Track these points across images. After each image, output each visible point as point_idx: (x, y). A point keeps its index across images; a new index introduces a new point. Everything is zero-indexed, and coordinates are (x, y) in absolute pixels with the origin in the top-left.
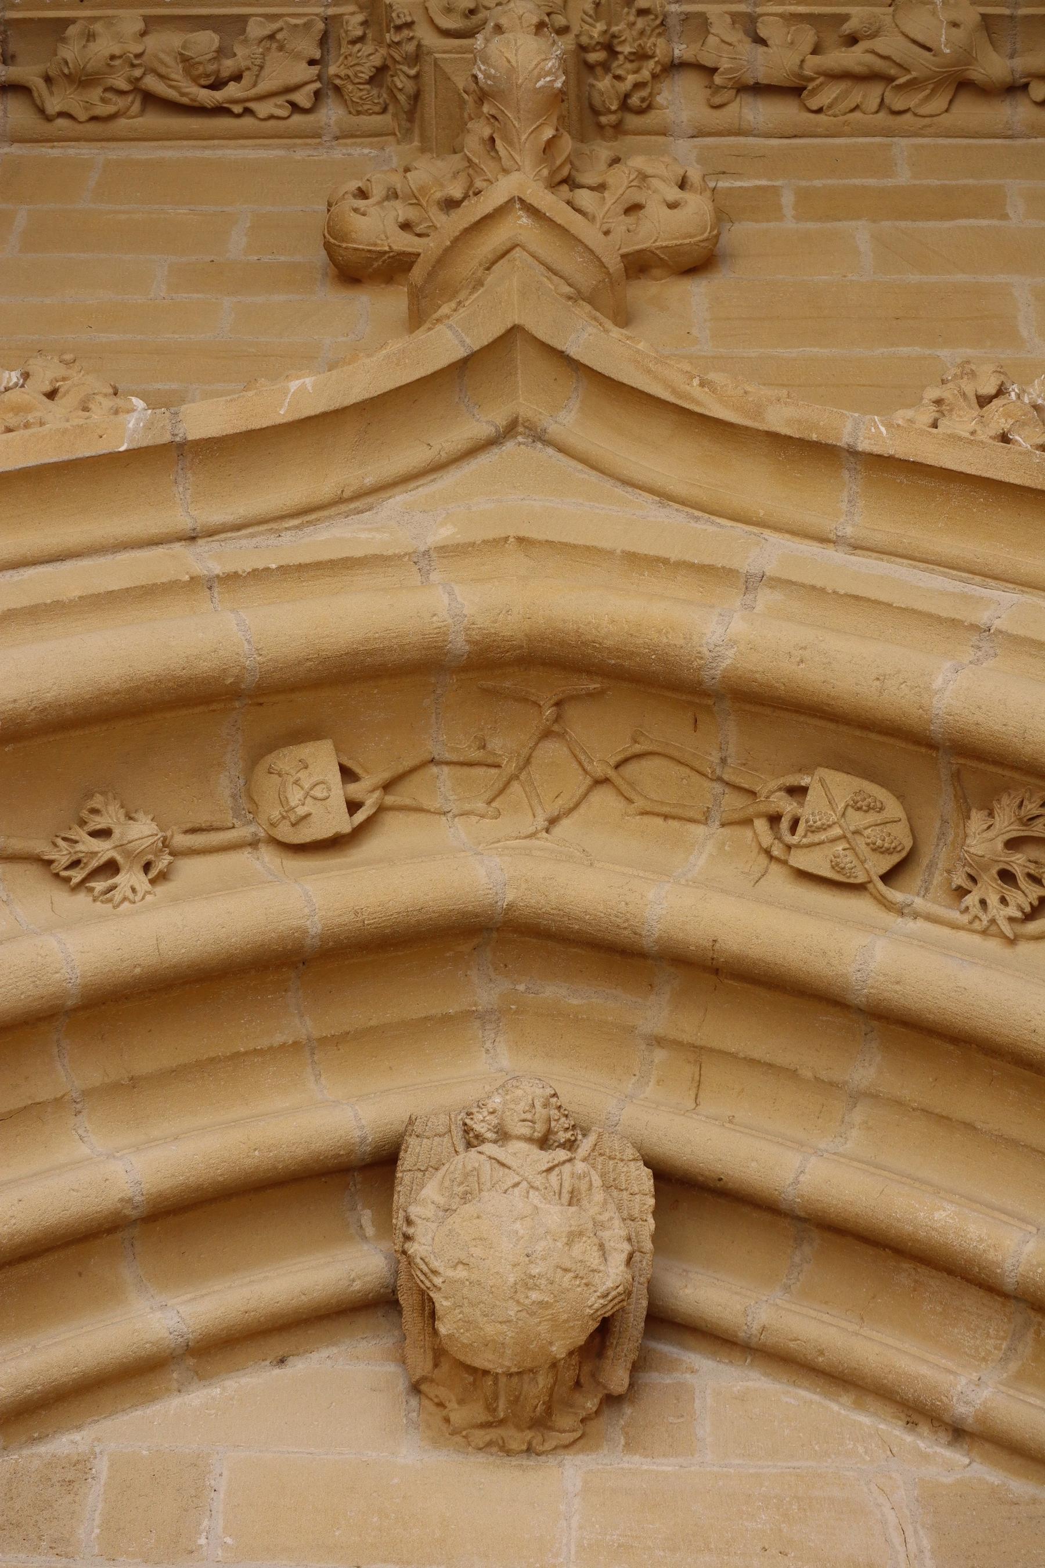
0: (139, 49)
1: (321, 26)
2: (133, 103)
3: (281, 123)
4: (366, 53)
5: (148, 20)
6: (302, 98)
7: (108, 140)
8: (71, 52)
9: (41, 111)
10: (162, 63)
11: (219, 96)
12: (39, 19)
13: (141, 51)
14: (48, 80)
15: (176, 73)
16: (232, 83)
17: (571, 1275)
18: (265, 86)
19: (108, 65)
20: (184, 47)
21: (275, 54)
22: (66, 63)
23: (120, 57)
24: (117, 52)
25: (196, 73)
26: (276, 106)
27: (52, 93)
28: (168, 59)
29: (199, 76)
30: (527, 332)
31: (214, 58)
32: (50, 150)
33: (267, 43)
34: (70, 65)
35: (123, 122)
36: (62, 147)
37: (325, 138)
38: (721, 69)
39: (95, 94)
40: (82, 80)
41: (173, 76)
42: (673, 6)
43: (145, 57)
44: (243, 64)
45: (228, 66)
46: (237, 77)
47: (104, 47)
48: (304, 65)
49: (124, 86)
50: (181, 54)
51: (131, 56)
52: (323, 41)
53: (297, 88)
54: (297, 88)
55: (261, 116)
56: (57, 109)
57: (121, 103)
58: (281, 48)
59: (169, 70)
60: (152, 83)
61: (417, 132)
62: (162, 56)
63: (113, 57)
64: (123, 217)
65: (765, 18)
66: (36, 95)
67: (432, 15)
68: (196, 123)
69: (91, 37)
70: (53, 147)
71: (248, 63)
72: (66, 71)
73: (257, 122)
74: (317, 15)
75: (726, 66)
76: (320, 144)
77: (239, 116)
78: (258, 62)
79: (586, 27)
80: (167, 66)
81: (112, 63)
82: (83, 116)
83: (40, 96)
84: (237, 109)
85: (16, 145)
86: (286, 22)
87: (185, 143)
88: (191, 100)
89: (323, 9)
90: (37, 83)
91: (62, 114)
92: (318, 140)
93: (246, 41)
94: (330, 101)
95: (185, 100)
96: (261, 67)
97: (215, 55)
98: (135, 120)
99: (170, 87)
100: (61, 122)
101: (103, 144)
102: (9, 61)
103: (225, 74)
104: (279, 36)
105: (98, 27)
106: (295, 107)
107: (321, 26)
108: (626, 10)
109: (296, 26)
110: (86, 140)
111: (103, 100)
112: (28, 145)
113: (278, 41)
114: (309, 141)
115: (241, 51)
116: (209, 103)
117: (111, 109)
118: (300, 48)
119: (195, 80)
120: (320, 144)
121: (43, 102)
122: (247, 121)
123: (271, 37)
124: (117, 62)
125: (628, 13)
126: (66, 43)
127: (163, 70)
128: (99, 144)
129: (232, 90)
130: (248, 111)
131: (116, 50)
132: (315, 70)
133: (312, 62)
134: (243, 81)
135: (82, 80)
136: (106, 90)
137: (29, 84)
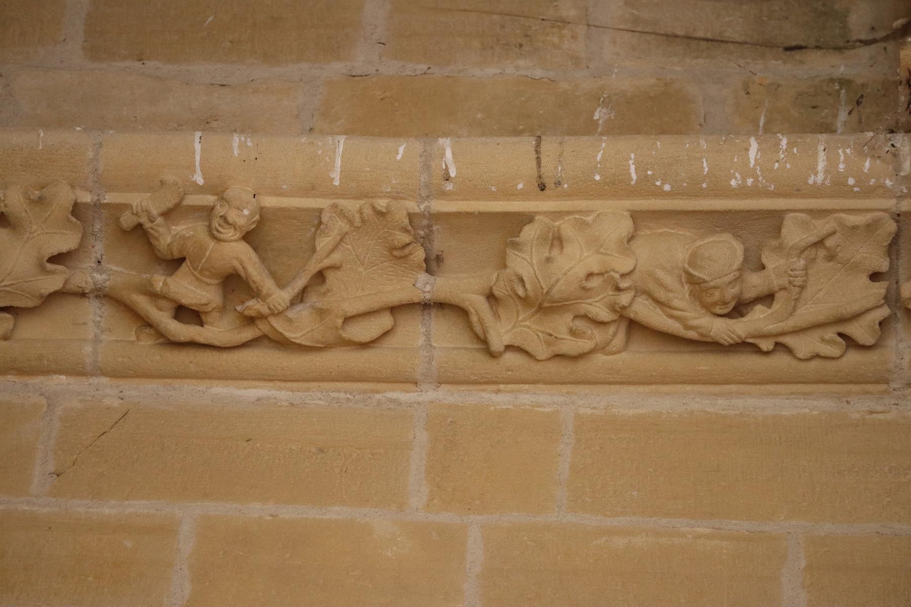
0: (625, 265)
1: (892, 227)
2: (615, 334)
3: (830, 365)
5: (636, 216)
6: (860, 331)
7: (578, 383)
8: (525, 263)
9: (483, 342)
10: (661, 285)
11: (740, 328)
12: (481, 214)
13: (630, 268)
14: (491, 297)
15: (681, 298)
16: (759, 308)
18: (807, 313)
19: (583, 288)
20: (693, 260)
21: (822, 265)
22: (521, 280)
23: (600, 274)
24: (596, 269)
25: (709, 300)
26: (823, 340)
27: (497, 316)
28: (668, 280)
29: (715, 304)
31: (736, 280)
32: (493, 397)
33: (810, 253)
34: (528, 286)
35: (600, 359)
36: (511, 392)
37: (894, 385)
39: (562, 324)
40: (544, 305)
41: (676, 303)
43: (635, 276)
44: (776, 283)
45: (755, 283)
46: (768, 298)
47: (575, 262)
48: (864, 279)
49: (604, 314)
50: (688, 274)
51: (617, 276)
52: (893, 248)
53: (855, 317)
54: (855, 317)
55: (800, 355)
56: (507, 340)
57: (599, 335)
58: (831, 257)
59: (671, 295)
60: (644, 311)
62: (661, 274)
63: (590, 275)
64: (620, 542)
66: (474, 319)
68: (705, 363)
69: (557, 240)
70: (498, 392)
71: (784, 281)
72: (521, 292)
73: (794, 363)
74: (885, 211)
76: (885, 392)
77: (767, 353)
78: (799, 281)
80: (668, 290)
81: (590, 284)
82: (542, 352)
83: (481, 322)
84: (766, 345)
85: (445, 387)
86: (841, 223)
87: (689, 388)
88: (701, 335)
89: (894, 201)
90: (477, 303)
91: (509, 348)
92: (883, 387)
93: (780, 248)
94: (899, 326)
95: (692, 335)
96: (802, 287)
97: (737, 274)
98: (617, 356)
99: (671, 317)
100: (511, 358)
101: (571, 388)
102: (434, 264)
103: (750, 294)
104: (829, 243)
105: (567, 228)
106: (850, 342)
107: (892, 227)
109: (855, 228)
110: (546, 383)
111: (573, 332)
112: (463, 388)
113: (826, 248)
114: (869, 387)
115: (772, 261)
116: (726, 339)
117: (584, 345)
118: (858, 257)
119: (708, 308)
120: (885, 392)
121: (485, 332)
122: (780, 361)
123: (820, 243)
124: (595, 283)
126: (520, 250)
127: (661, 295)
128: (564, 389)
129: (759, 319)
130: (780, 347)
131: (593, 263)
132: (880, 288)
133: (875, 276)
134: (776, 306)
135: (544, 305)
136: (576, 317)
137: (466, 305)
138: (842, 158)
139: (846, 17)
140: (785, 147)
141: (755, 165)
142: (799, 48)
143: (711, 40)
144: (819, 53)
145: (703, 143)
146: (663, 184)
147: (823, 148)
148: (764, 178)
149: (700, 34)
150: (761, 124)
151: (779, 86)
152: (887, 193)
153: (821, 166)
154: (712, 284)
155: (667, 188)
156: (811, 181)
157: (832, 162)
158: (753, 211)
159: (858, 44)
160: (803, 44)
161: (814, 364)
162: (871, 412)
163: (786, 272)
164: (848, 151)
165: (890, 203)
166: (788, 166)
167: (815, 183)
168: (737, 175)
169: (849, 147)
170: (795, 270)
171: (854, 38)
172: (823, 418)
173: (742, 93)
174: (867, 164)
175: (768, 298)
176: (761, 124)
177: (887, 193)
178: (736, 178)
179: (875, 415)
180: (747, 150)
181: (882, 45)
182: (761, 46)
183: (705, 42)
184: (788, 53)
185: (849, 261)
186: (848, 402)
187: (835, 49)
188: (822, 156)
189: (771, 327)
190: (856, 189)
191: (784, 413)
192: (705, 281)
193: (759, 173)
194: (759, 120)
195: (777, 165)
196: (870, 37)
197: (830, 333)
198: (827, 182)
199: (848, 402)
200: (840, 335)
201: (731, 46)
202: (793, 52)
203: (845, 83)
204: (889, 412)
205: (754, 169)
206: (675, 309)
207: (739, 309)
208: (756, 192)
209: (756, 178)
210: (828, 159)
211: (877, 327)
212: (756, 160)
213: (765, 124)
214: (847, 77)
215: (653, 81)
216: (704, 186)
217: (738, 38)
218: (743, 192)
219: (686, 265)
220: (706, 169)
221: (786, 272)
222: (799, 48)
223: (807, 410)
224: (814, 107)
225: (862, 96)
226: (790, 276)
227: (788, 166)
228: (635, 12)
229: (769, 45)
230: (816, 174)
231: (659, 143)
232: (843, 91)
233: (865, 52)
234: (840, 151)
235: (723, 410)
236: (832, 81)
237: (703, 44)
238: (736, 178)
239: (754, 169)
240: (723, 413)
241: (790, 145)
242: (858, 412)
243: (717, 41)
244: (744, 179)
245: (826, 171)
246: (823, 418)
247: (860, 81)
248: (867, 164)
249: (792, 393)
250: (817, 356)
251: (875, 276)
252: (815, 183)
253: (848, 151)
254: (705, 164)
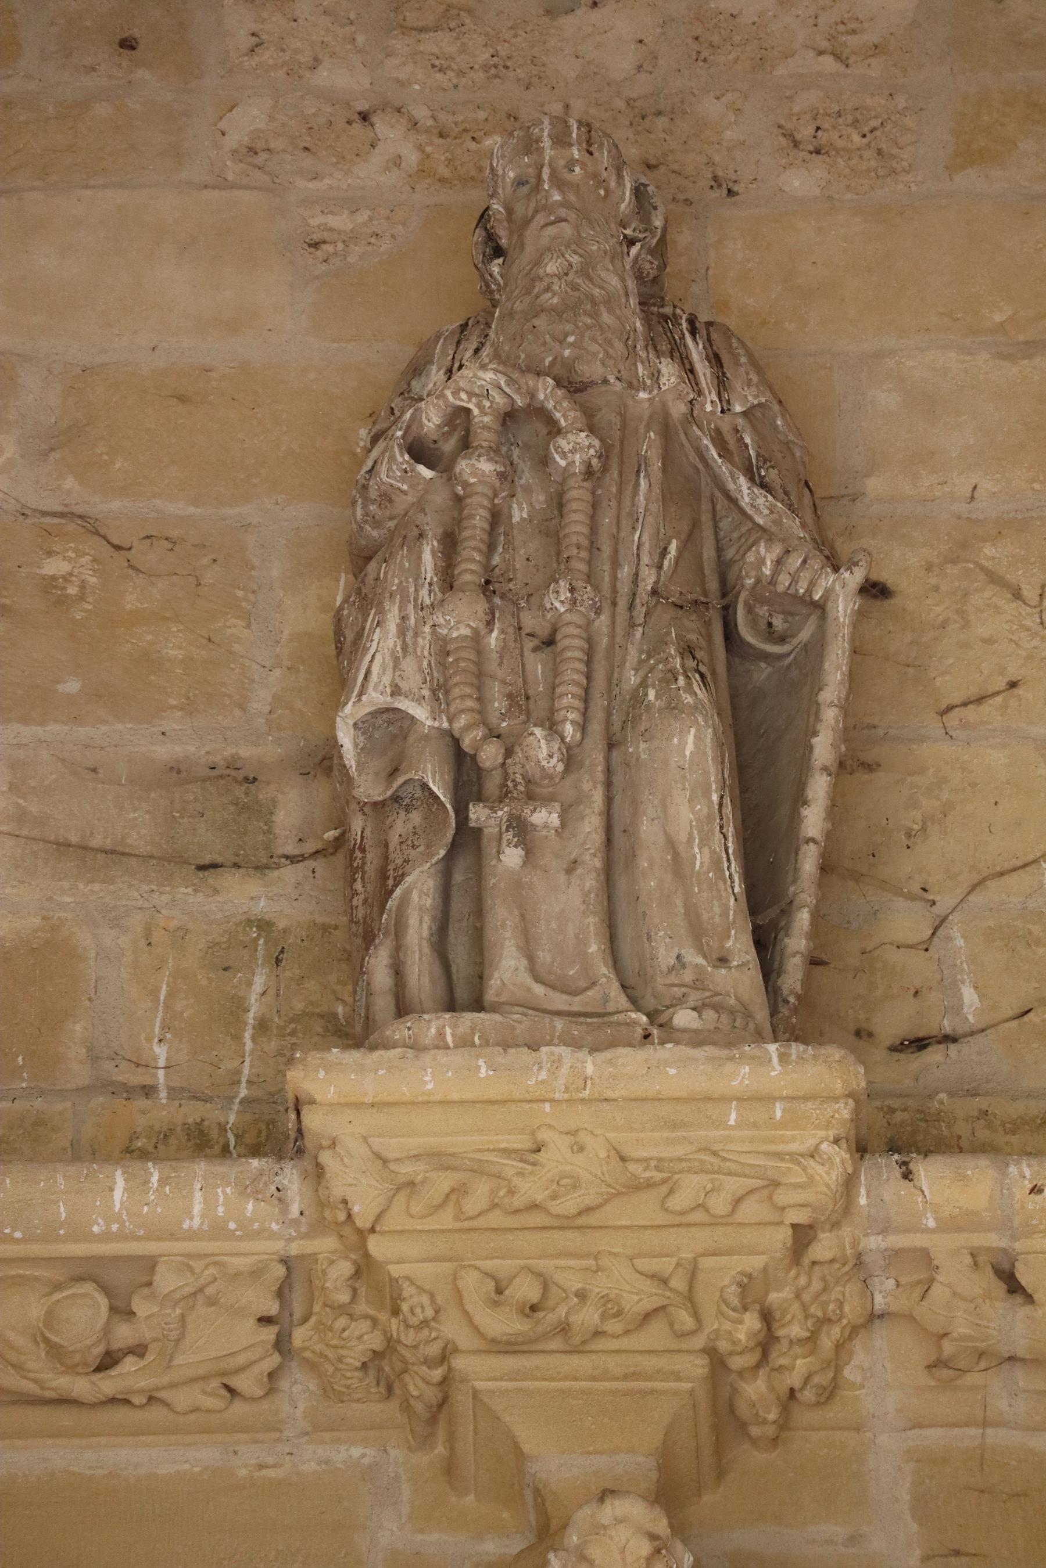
1: (281, 1271)
4: (357, 1333)
11: (108, 1385)
15: (37, 1361)
16: (130, 1359)
17: (841, 1298)
20: (50, 1317)
28: (20, 1341)
30: (606, 1049)
38: (955, 1334)
41: (30, 1365)
42: (873, 1238)
46: (139, 1350)
48: (251, 1322)
52: (281, 1293)
58: (212, 1302)
59: (23, 1358)
61: (441, 1435)
62: (12, 1336)
65: (1031, 1257)
67: (469, 1308)
68: (65, 1418)
75: (961, 1330)
77: (141, 1407)
79: (727, 1326)
84: (137, 1400)
93: (153, 1296)
95: (49, 1394)
104: (210, 1291)
108: (793, 1272)
109: (238, 1275)
115: (142, 1307)
122: (156, 1414)
125: (797, 1277)
132: (269, 1334)
133: (265, 1320)
134: (150, 1357)
138: (221, 1199)
139: (272, 813)
140: (155, 1185)
141: (121, 1209)
142: (214, 866)
143: (113, 852)
144: (238, 874)
145: (60, 1179)
146: (13, 1231)
147: (199, 1186)
148: (131, 1223)
149: (97, 841)
150: (162, 998)
151: (187, 931)
152: (274, 1236)
153: (197, 1209)
154: (70, 1349)
155: (18, 1235)
156: (186, 1226)
157: (209, 1204)
158: (120, 1257)
159: (283, 860)
160: (219, 860)
161: (193, 1417)
162: (261, 1467)
163: (159, 1324)
164: (228, 1190)
165: (278, 1246)
166: (159, 1210)
167: (190, 1227)
168: (100, 1221)
169: (229, 1184)
170: (170, 1324)
171: (280, 851)
172: (206, 1477)
173: (142, 944)
174: (250, 1206)
175: (139, 1350)
176: (162, 998)
177: (274, 1236)
178: (98, 1224)
179: (264, 1472)
180: (112, 1190)
181: (311, 864)
182: (169, 861)
183: (104, 855)
184: (201, 874)
185: (232, 1306)
186: (235, 1452)
187: (257, 868)
188: (198, 1196)
189: (143, 1384)
190: (238, 1233)
191: (162, 1471)
192: (62, 1346)
193: (125, 1218)
194: (158, 989)
195: (146, 1208)
196: (297, 852)
197: (215, 1384)
198: (205, 1227)
199: (235, 1452)
200: (227, 1387)
201: (134, 862)
202: (206, 873)
203: (264, 925)
204: (282, 1465)
205: (120, 1214)
206: (29, 1371)
207: (108, 1362)
208: (122, 1237)
209: (122, 1223)
210: (206, 1201)
211: (265, 1379)
212: (122, 1203)
213: (166, 997)
214: (267, 918)
215: (37, 921)
216: (62, 1232)
217: (145, 849)
218: (107, 1237)
219: (41, 1325)
220: (64, 1215)
221: (159, 1324)
222: (214, 866)
223: (187, 1466)
224: (225, 969)
225: (282, 952)
226: (164, 1329)
227: (159, 1210)
228: (21, 801)
229: (178, 859)
230: (192, 1218)
231: (8, 1181)
232: (261, 941)
233: (290, 874)
234: (219, 1191)
235: (90, 1468)
236: (249, 922)
237: (101, 857)
238: (98, 1224)
239: (120, 1214)
240: (89, 1472)
241: (163, 1181)
242: (246, 1466)
243: (116, 854)
244: (108, 1225)
245: (203, 1216)
246: (206, 1477)
247: (281, 924)
248: (250, 1206)
249: (170, 1445)
250: (196, 1410)
251: (265, 1320)
252: (190, 1227)
253: (228, 1190)
254: (62, 1209)
